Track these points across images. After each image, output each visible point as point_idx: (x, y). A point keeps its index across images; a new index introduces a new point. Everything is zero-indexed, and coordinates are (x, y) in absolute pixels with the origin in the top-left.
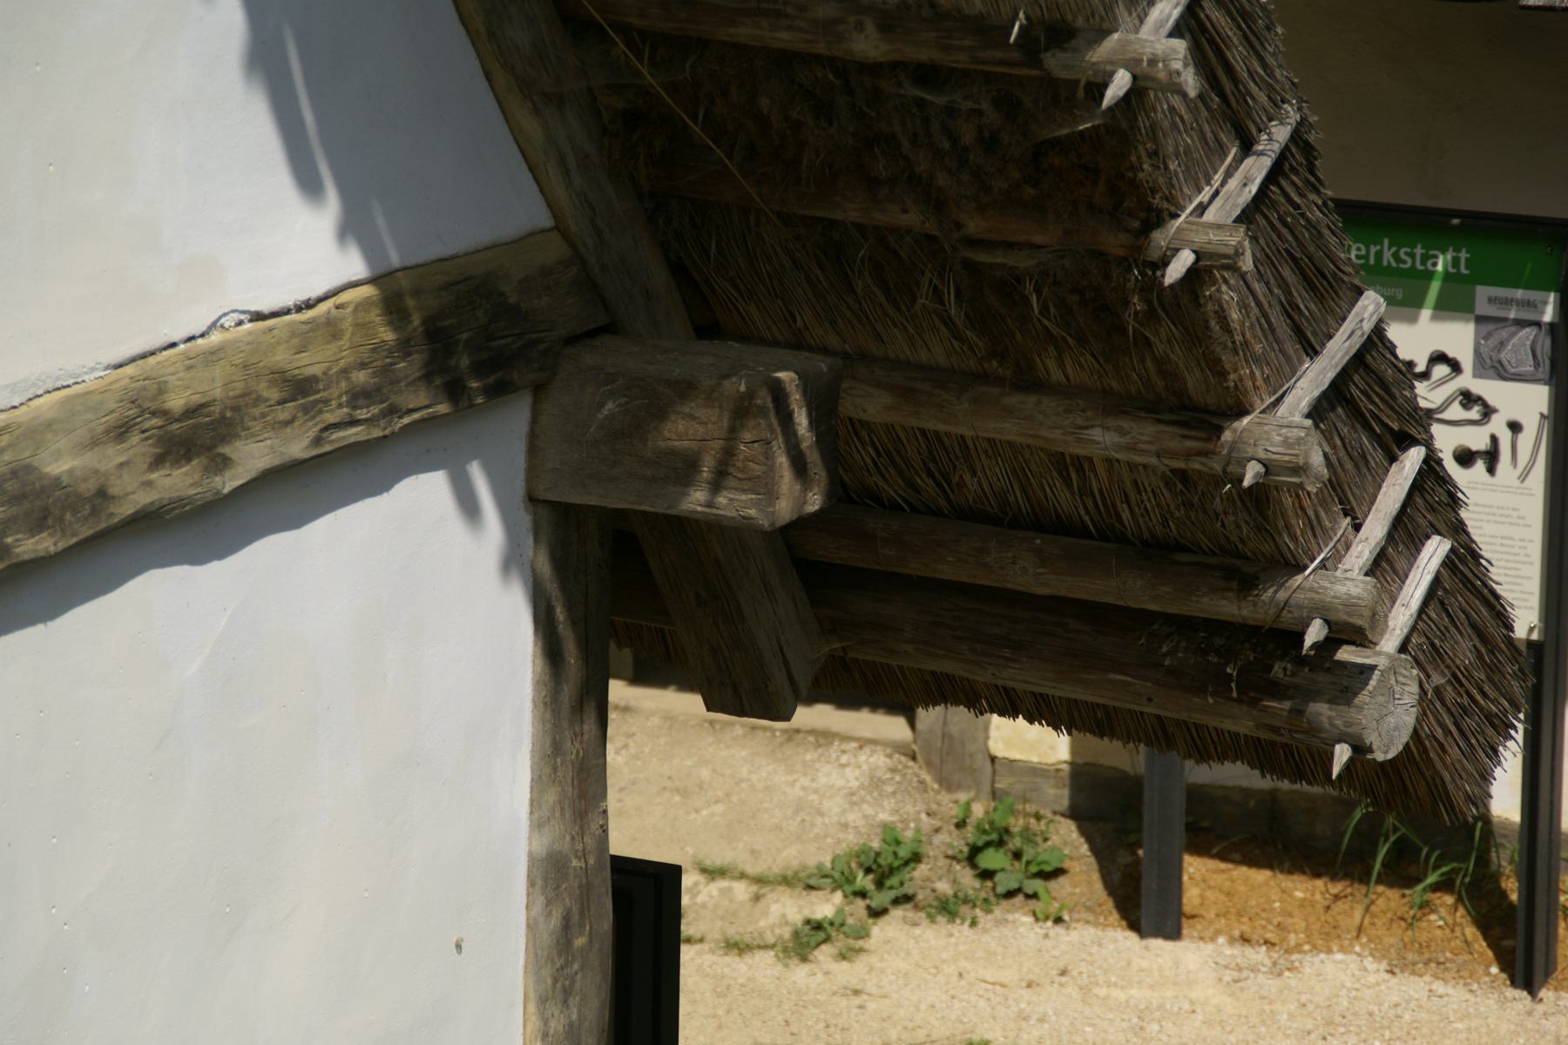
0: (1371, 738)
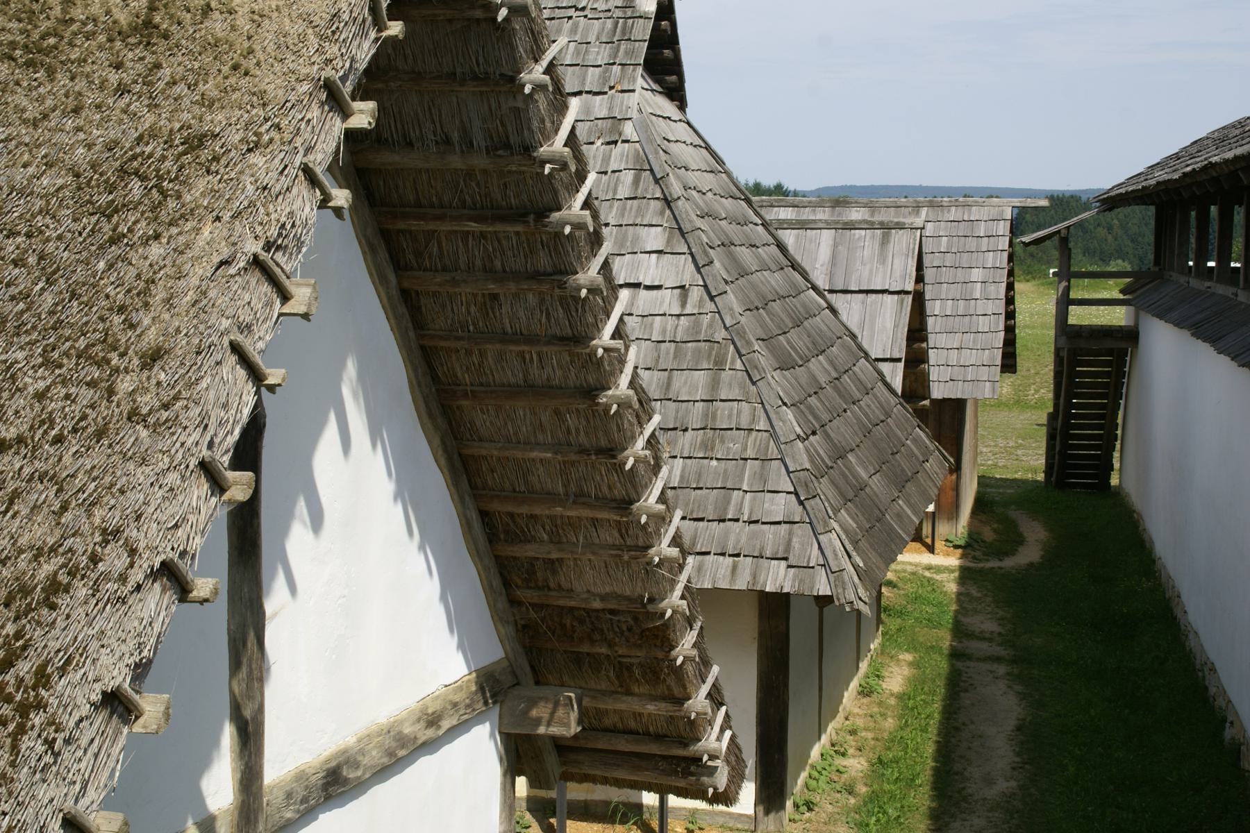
0: (719, 786)
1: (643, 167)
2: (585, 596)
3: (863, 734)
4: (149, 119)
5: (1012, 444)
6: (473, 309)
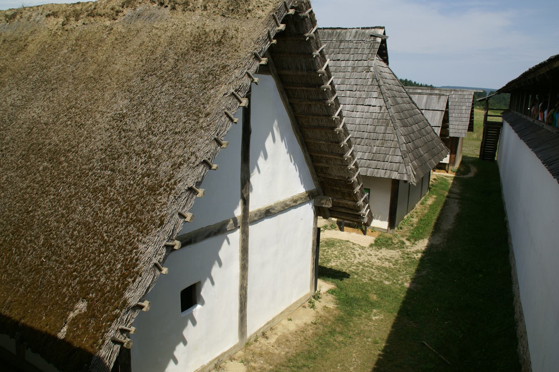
1: (374, 78)
2: (334, 176)
3: (419, 213)
4: (217, 62)
5: (474, 149)
6: (306, 108)
